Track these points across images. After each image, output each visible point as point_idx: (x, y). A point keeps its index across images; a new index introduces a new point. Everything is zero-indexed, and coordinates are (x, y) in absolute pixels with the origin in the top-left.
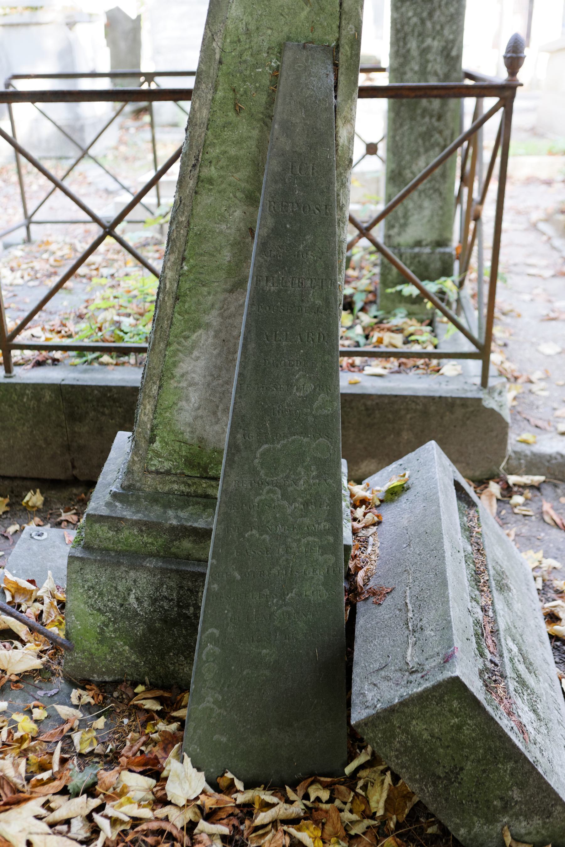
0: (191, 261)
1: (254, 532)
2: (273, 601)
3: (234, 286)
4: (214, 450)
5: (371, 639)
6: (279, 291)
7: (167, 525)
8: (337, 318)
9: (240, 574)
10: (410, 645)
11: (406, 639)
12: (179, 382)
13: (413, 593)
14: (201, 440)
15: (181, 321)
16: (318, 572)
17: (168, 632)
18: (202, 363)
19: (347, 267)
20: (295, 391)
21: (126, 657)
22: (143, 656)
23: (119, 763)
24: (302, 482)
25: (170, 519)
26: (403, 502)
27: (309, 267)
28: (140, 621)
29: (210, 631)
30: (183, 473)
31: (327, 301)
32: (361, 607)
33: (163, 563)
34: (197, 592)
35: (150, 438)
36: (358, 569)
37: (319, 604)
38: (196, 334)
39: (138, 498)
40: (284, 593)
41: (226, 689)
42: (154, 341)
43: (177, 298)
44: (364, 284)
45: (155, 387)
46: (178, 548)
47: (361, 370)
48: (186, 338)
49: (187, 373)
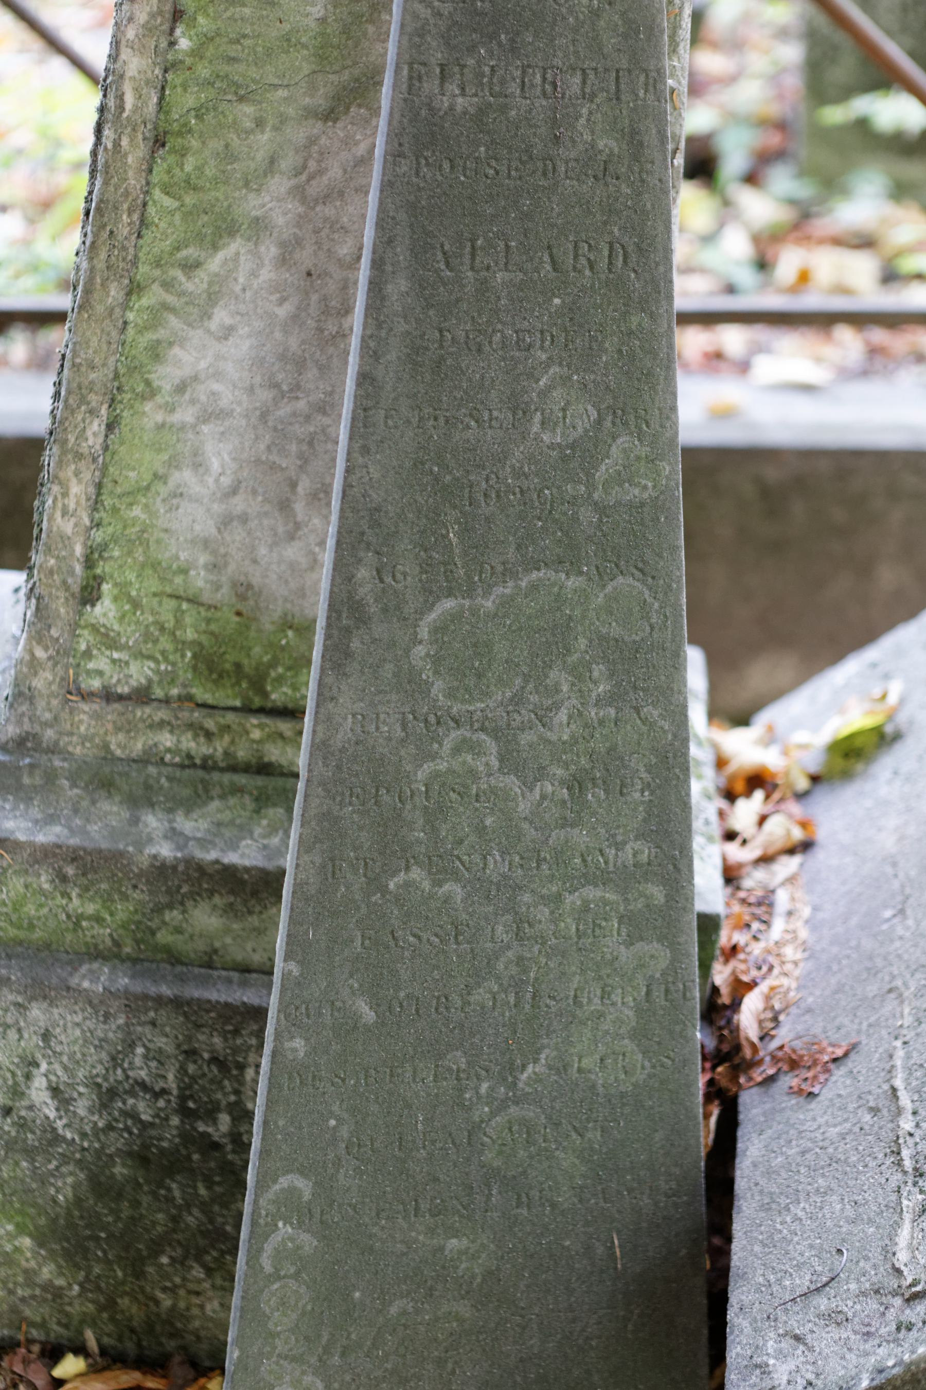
0: (201, 20)
1: (416, 873)
2: (477, 1089)
3: (337, 98)
4: (286, 624)
5: (783, 1201)
6: (482, 111)
7: (144, 861)
8: (666, 192)
9: (375, 1006)
10: (908, 1217)
11: (894, 1197)
12: (171, 409)
13: (916, 1058)
14: (244, 590)
15: (172, 213)
16: (617, 997)
17: (154, 1194)
18: (241, 346)
19: (696, 39)
20: (536, 428)
21: (26, 1271)
22: (77, 1266)
23: (166, 695)
24: (563, 716)
25: (150, 840)
26: (883, 777)
27: (576, 30)
28: (65, 1159)
29: (284, 1182)
30: (189, 698)
31: (635, 142)
32: (751, 1105)
33: (133, 977)
34: (241, 1067)
35: (84, 588)
36: (741, 988)
37: (623, 1095)
38: (221, 255)
39: (51, 777)
40: (512, 1063)
41: (336, 1360)
42: (90, 281)
43: (159, 142)
44: (751, 95)
45: (96, 427)
46: (178, 930)
47: (743, 367)
48: (190, 267)
49: (195, 378)
